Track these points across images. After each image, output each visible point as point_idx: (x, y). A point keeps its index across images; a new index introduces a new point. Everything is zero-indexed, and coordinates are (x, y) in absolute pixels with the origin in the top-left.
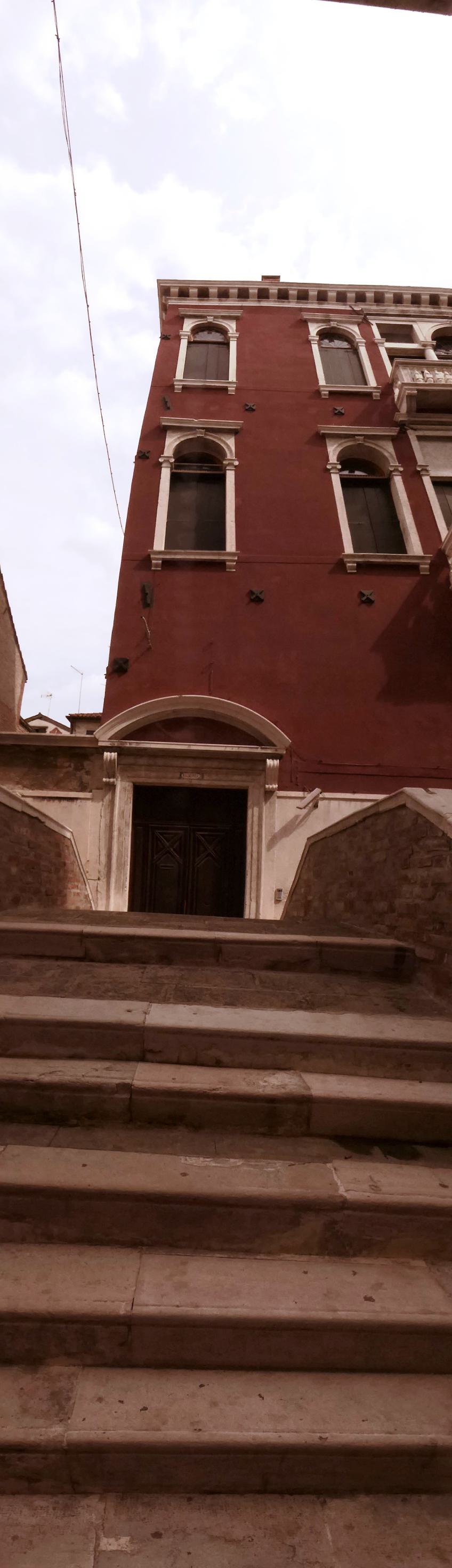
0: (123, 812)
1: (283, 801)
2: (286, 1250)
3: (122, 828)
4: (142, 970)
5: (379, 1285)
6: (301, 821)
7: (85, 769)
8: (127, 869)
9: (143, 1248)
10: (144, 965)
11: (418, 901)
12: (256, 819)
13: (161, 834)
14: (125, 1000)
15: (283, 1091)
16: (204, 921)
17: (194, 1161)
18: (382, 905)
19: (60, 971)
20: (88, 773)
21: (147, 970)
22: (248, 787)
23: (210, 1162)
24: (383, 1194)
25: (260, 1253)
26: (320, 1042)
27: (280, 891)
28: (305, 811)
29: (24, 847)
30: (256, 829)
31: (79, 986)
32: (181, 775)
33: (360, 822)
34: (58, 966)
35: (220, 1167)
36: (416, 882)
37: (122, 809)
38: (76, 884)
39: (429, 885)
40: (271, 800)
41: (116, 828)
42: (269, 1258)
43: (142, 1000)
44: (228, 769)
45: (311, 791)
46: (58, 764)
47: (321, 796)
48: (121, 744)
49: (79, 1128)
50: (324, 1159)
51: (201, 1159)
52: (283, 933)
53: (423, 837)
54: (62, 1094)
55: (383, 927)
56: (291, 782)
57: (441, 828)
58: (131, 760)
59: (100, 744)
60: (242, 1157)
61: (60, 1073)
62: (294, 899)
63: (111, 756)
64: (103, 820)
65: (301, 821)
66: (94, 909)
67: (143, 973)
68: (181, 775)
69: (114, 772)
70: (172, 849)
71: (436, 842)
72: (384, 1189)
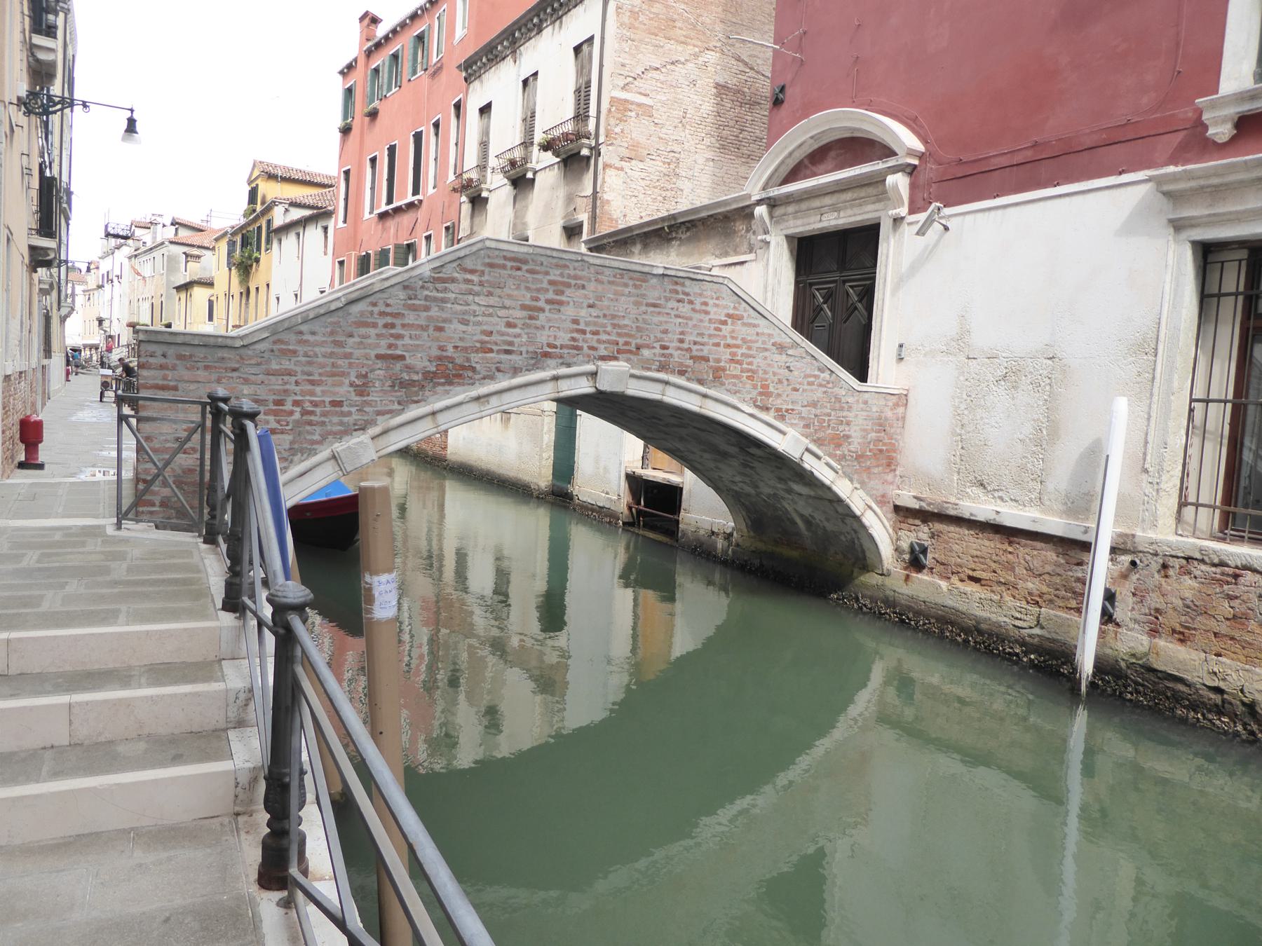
6: (931, 252)
13: (818, 290)
22: (880, 217)
40: (901, 229)
41: (770, 288)
65: (931, 252)
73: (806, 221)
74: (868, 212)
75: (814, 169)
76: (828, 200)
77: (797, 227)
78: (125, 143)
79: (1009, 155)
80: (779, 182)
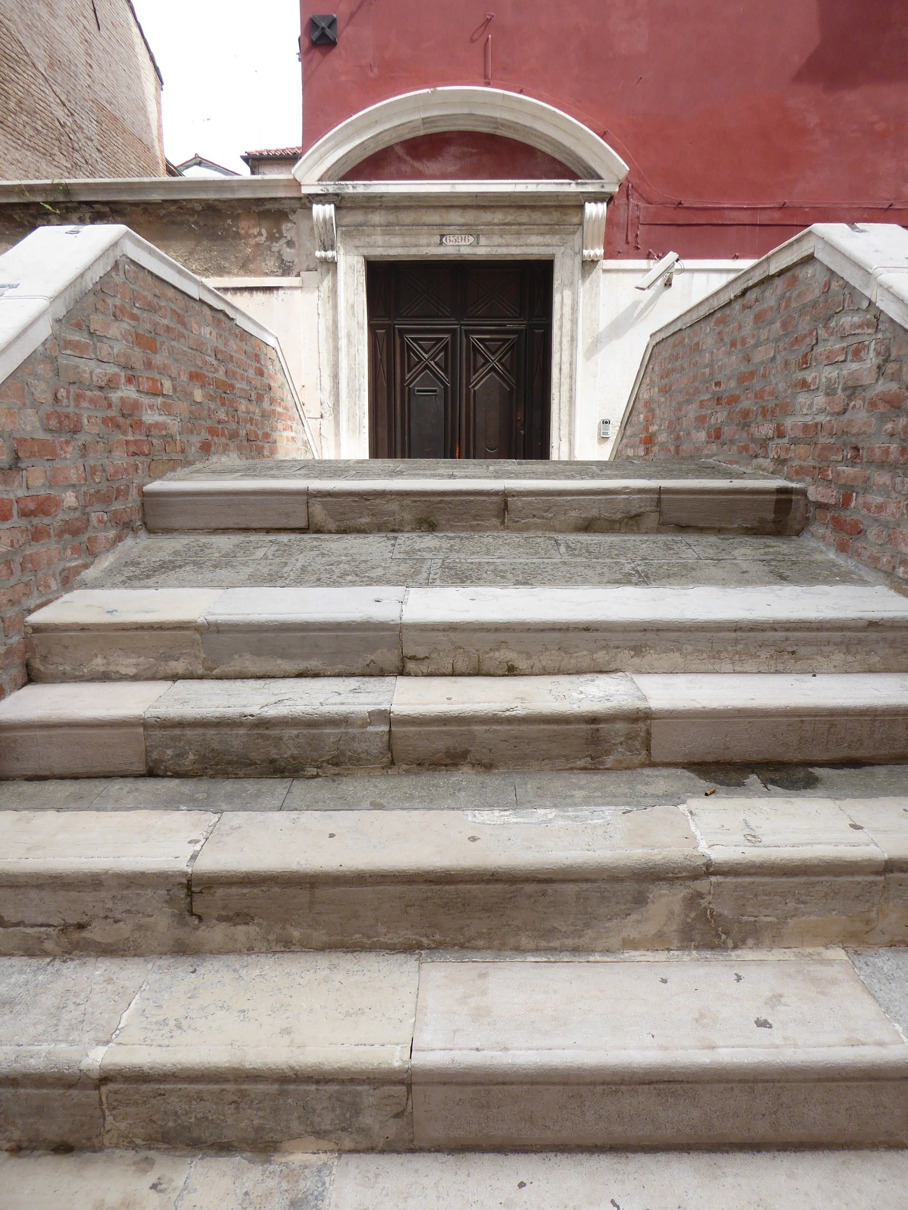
0: (353, 306)
1: (613, 276)
2: (631, 944)
3: (353, 334)
4: (393, 542)
5: (776, 1000)
7: (286, 237)
8: (364, 397)
9: (423, 952)
10: (396, 535)
11: (822, 418)
12: (567, 310)
14: (370, 585)
15: (609, 705)
16: (488, 467)
17: (486, 818)
18: (766, 429)
19: (274, 548)
20: (290, 244)
21: (399, 541)
23: (509, 817)
24: (765, 846)
25: (593, 951)
26: (658, 630)
27: (606, 423)
28: (649, 293)
29: (207, 358)
30: (567, 326)
31: (304, 569)
32: (441, 240)
33: (737, 297)
34: (271, 541)
35: (524, 823)
36: (818, 388)
37: (351, 302)
38: (289, 423)
39: (839, 391)
40: (593, 275)
41: (342, 333)
42: (606, 959)
43: (397, 584)
44: (520, 224)
45: (660, 258)
46: (242, 232)
47: (677, 266)
48: (339, 189)
49: (320, 779)
50: (673, 798)
51: (496, 813)
52: (609, 477)
53: (837, 313)
54: (295, 732)
55: (766, 463)
56: (627, 243)
57: (867, 293)
58: (357, 217)
59: (305, 190)
60: (555, 806)
61: (289, 703)
62: (628, 432)
63: (324, 212)
64: (322, 320)
66: (317, 458)
67: (393, 545)
68: (441, 240)
69: (333, 241)
70: (432, 363)
71: (856, 319)
72: (766, 840)
73: (409, 240)
74: (533, 245)
75: (418, 165)
76: (455, 217)
77: (391, 247)
78: (308, 19)
79: (749, 212)
80: (342, 174)
